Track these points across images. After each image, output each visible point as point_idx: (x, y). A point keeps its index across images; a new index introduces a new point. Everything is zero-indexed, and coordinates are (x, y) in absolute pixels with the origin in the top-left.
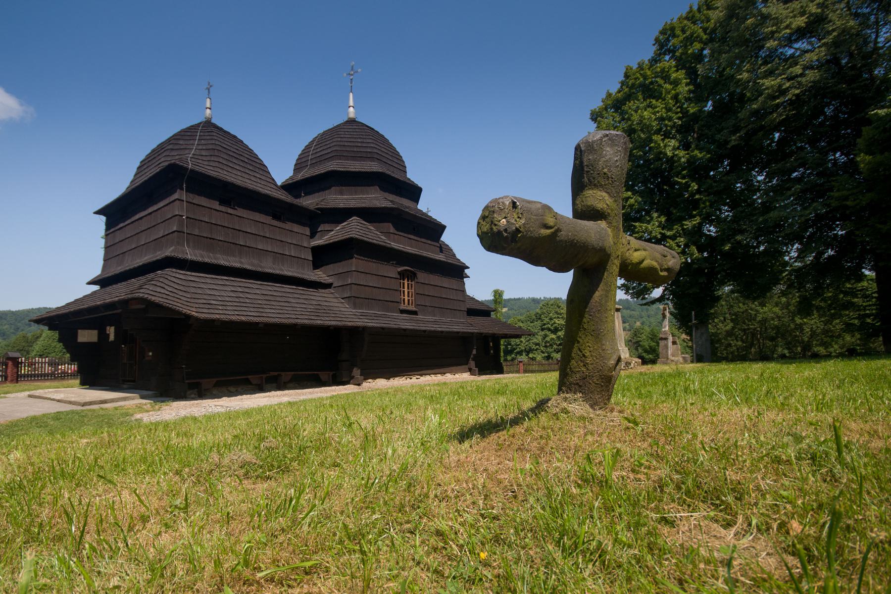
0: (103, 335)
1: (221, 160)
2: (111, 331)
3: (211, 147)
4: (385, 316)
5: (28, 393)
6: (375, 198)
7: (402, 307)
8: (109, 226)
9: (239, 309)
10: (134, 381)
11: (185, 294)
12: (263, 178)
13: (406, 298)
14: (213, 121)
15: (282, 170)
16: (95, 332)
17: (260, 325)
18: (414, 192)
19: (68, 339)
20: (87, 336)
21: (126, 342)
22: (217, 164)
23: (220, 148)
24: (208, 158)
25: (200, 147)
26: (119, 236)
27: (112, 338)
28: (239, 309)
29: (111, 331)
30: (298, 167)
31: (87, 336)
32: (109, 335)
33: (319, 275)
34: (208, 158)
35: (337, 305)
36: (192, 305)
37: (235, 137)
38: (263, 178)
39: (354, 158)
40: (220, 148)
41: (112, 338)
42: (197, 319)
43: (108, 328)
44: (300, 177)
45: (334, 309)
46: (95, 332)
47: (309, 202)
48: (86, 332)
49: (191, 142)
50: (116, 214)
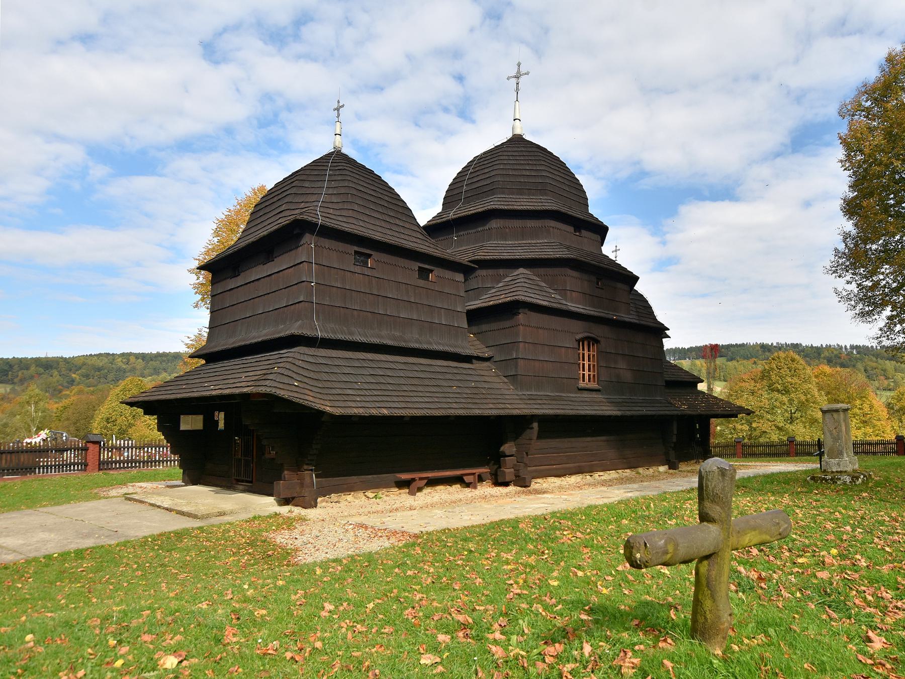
0: (210, 422)
1: (356, 208)
2: (220, 417)
3: (343, 191)
4: (560, 398)
5: (124, 490)
6: (551, 243)
7: (582, 384)
8: (213, 282)
9: (380, 399)
10: (251, 482)
11: (315, 383)
12: (407, 225)
13: (586, 373)
14: (344, 151)
15: (426, 208)
16: (200, 418)
17: (405, 419)
18: (601, 230)
19: (169, 426)
20: (190, 423)
21: (232, 431)
22: (350, 213)
23: (355, 192)
24: (340, 206)
25: (330, 191)
26: (228, 300)
27: (221, 425)
28: (380, 399)
29: (220, 417)
30: (450, 200)
31: (190, 423)
32: (217, 422)
33: (470, 345)
34: (340, 206)
35: (498, 386)
36: (325, 397)
37: (372, 172)
38: (407, 225)
39: (520, 192)
40: (355, 192)
41: (221, 425)
42: (332, 416)
43: (216, 413)
44: (451, 215)
45: (490, 393)
46: (200, 418)
47: (460, 249)
48: (190, 418)
49: (319, 184)
50: (221, 269)
